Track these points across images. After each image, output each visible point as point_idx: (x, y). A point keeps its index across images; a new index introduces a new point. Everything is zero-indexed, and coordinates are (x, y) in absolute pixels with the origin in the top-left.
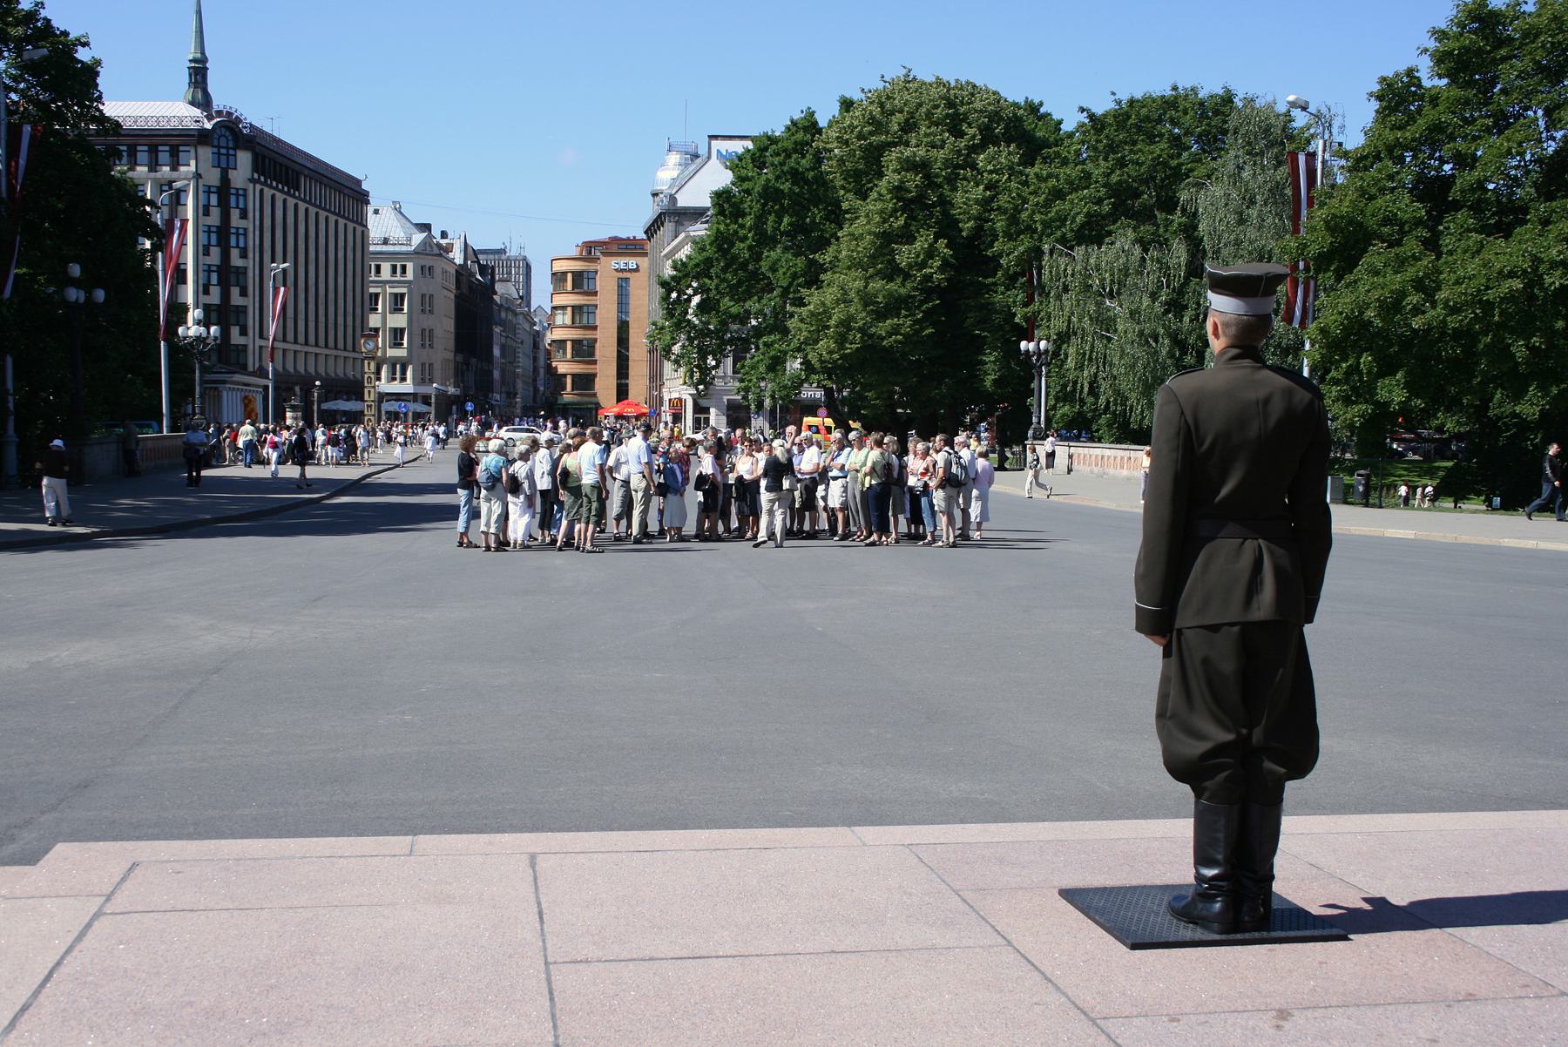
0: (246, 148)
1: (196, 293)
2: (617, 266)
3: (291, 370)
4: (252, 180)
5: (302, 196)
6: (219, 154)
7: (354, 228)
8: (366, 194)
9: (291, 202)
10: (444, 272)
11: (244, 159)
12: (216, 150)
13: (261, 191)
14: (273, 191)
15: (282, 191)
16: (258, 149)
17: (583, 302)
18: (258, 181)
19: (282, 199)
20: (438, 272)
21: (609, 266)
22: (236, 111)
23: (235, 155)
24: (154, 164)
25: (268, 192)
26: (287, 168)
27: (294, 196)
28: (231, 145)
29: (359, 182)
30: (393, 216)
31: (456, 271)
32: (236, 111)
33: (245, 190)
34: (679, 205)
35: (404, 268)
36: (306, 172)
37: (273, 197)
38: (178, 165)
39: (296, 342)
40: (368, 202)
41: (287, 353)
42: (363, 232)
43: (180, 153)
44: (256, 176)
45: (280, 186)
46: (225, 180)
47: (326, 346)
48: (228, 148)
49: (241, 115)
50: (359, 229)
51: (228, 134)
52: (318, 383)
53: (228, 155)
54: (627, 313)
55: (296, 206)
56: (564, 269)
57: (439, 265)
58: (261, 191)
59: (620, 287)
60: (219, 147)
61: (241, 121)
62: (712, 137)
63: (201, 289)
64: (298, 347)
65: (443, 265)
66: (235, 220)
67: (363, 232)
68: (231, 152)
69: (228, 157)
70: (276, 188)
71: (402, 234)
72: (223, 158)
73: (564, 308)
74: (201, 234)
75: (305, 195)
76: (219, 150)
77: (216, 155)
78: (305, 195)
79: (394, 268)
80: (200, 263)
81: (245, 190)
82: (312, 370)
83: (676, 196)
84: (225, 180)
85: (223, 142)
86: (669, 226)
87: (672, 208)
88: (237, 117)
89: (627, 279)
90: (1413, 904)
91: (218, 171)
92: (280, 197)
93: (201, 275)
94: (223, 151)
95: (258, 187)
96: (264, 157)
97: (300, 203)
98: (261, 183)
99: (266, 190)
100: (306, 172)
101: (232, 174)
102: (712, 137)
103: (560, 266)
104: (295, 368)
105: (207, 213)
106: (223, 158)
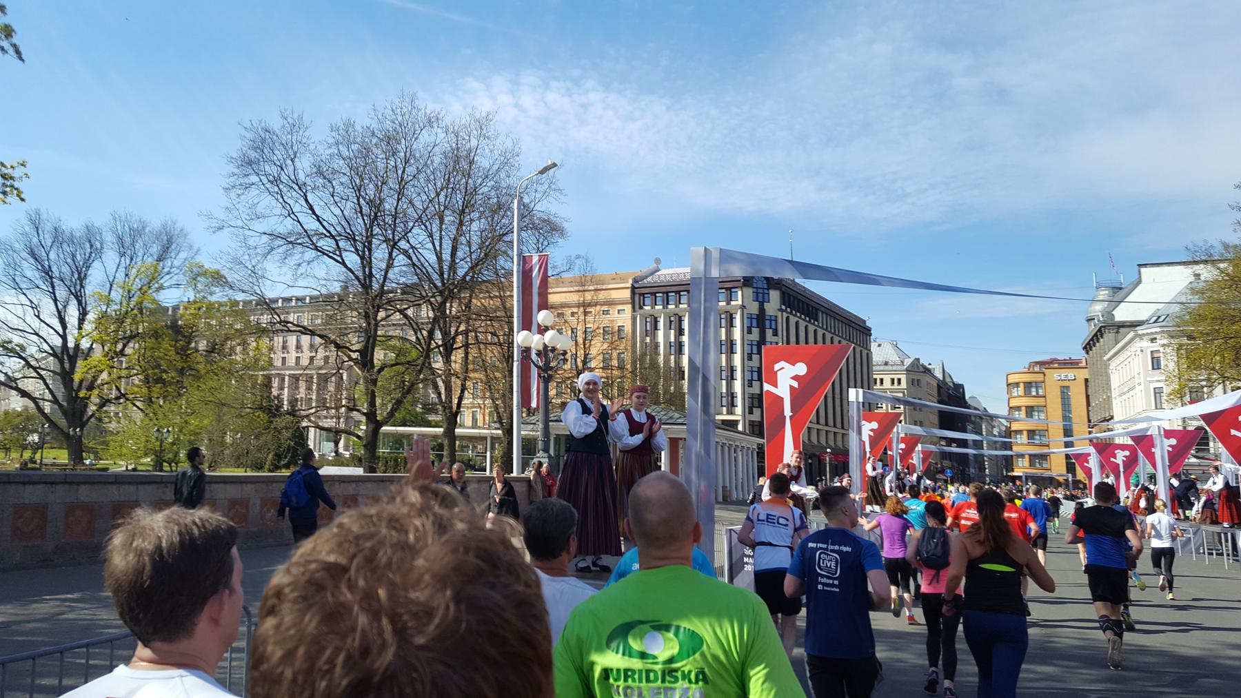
0: (776, 289)
1: (743, 385)
2: (1059, 378)
3: (815, 442)
4: (781, 310)
5: (821, 325)
6: (757, 293)
7: (861, 351)
8: (869, 330)
9: (811, 328)
10: (928, 384)
11: (775, 295)
12: (755, 290)
13: (788, 319)
14: (797, 319)
15: (805, 320)
16: (784, 289)
17: (1033, 404)
18: (786, 311)
20: (923, 383)
21: (1056, 375)
23: (768, 294)
25: (793, 320)
26: (808, 305)
27: (814, 324)
28: (765, 286)
29: (864, 322)
30: (891, 348)
31: (938, 385)
33: (776, 317)
35: (899, 380)
36: (823, 309)
37: (797, 323)
38: (731, 300)
39: (835, 426)
40: (870, 335)
41: (812, 430)
42: (868, 354)
44: (783, 307)
45: (794, 312)
46: (762, 310)
47: (827, 424)
50: (865, 352)
52: (828, 450)
53: (763, 293)
54: (1070, 411)
55: (815, 331)
56: (1017, 381)
57: (925, 378)
58: (788, 319)
59: (1062, 392)
62: (1140, 266)
63: (746, 383)
64: (836, 430)
65: (927, 379)
67: (868, 354)
68: (766, 291)
70: (800, 318)
71: (898, 359)
72: (760, 295)
73: (1017, 385)
74: (745, 345)
75: (823, 325)
78: (823, 325)
79: (893, 380)
80: (746, 365)
81: (776, 317)
82: (824, 443)
83: (1113, 313)
84: (762, 310)
86: (1109, 336)
89: (1068, 387)
91: (757, 304)
92: (802, 324)
95: (785, 315)
96: (789, 296)
97: (827, 333)
98: (787, 312)
99: (791, 317)
100: (823, 309)
101: (766, 306)
102: (1140, 266)
103: (1012, 379)
104: (818, 441)
105: (750, 332)
106: (760, 295)
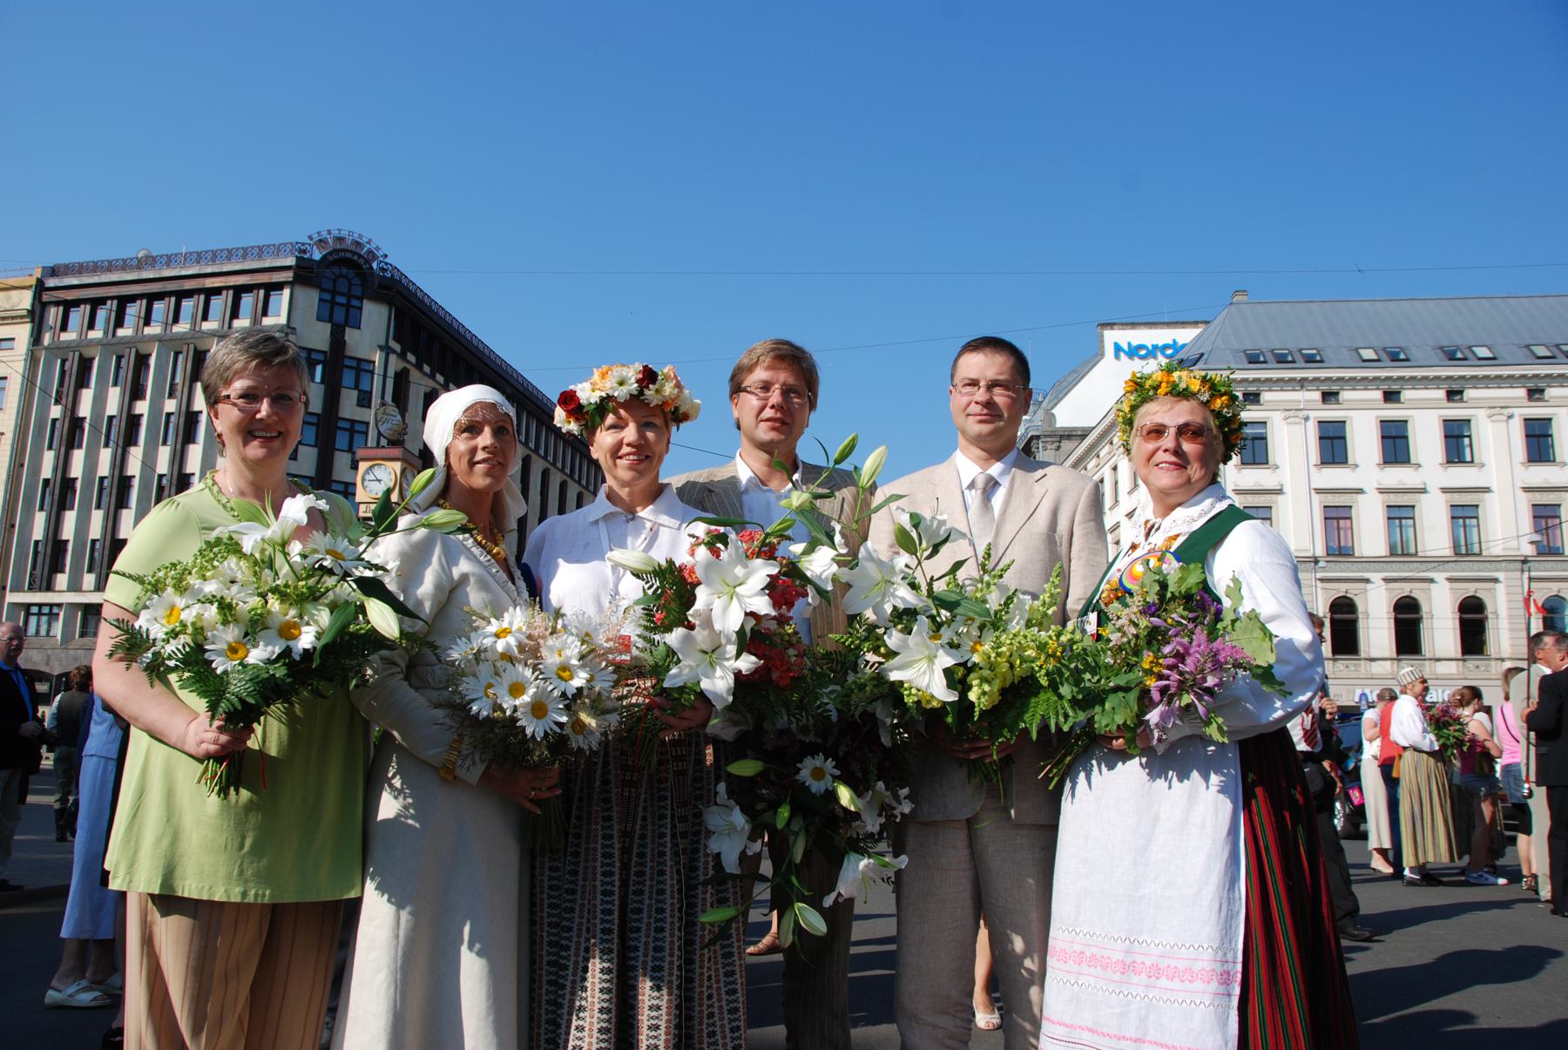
0: (377, 298)
6: (333, 303)
12: (327, 296)
19: (423, 390)
22: (369, 242)
23: (361, 309)
24: (260, 311)
32: (369, 242)
34: (854, 923)
43: (1526, 656)
48: (349, 296)
49: (378, 248)
51: (344, 271)
53: (348, 306)
60: (334, 293)
61: (375, 257)
66: (349, 407)
69: (347, 312)
76: (349, 301)
77: (328, 305)
85: (342, 286)
87: (1049, 429)
88: (370, 251)
90: (1391, 932)
93: (1476, 540)
94: (341, 300)
101: (351, 335)
